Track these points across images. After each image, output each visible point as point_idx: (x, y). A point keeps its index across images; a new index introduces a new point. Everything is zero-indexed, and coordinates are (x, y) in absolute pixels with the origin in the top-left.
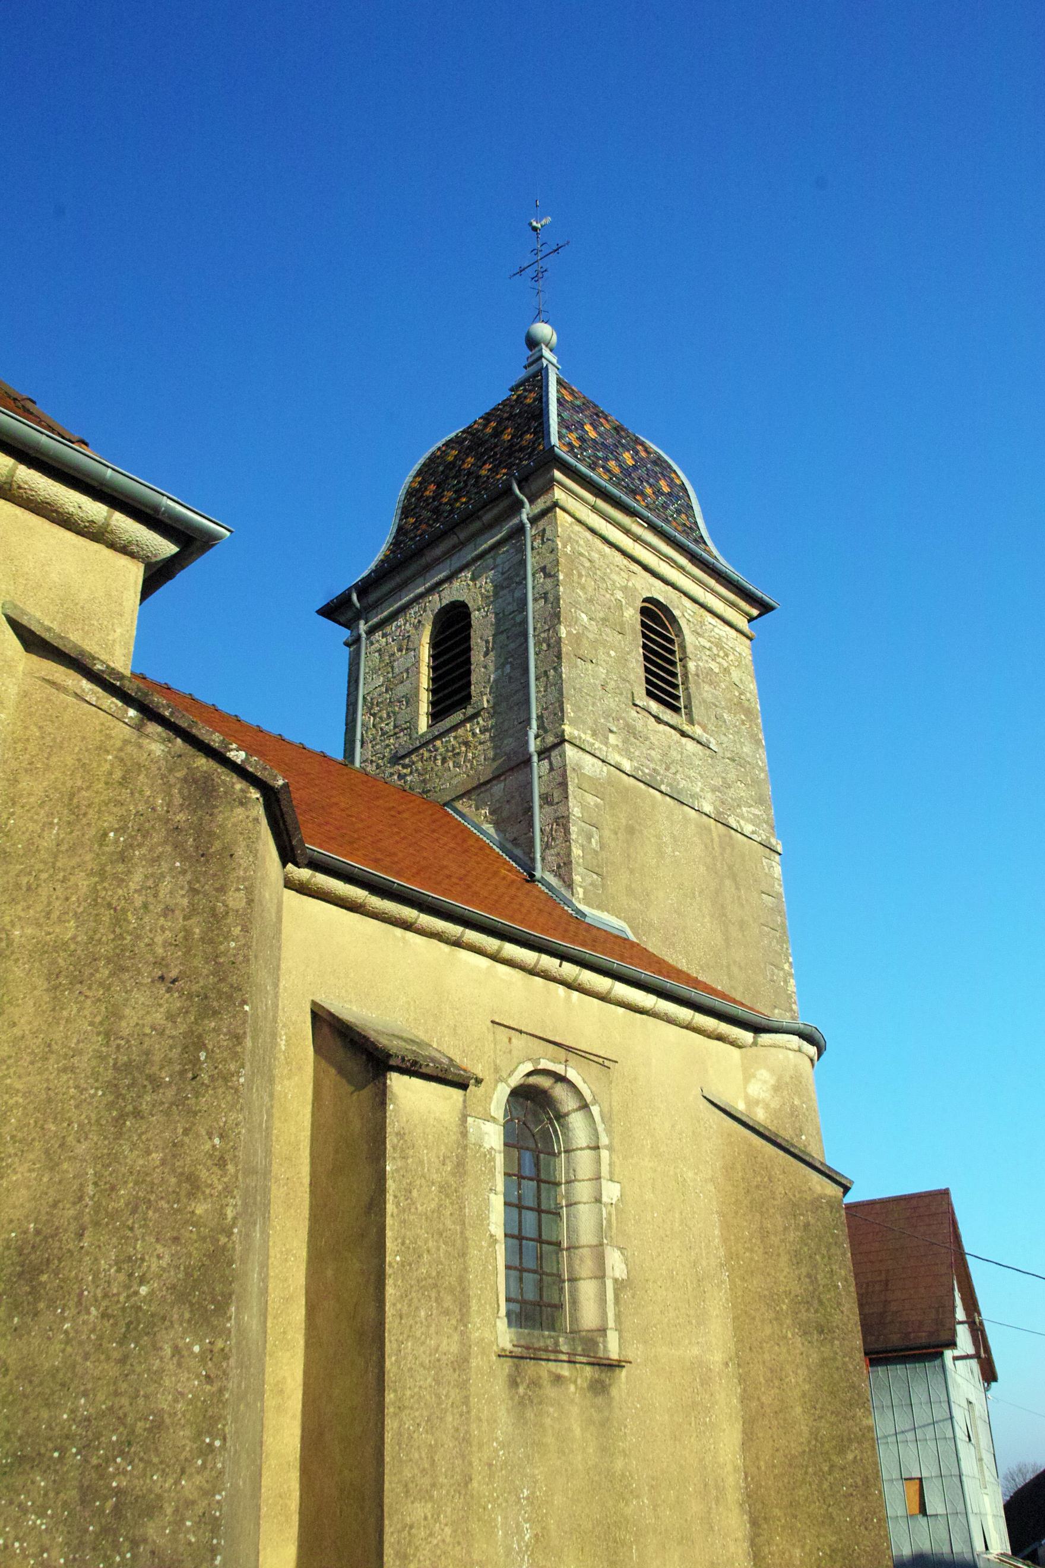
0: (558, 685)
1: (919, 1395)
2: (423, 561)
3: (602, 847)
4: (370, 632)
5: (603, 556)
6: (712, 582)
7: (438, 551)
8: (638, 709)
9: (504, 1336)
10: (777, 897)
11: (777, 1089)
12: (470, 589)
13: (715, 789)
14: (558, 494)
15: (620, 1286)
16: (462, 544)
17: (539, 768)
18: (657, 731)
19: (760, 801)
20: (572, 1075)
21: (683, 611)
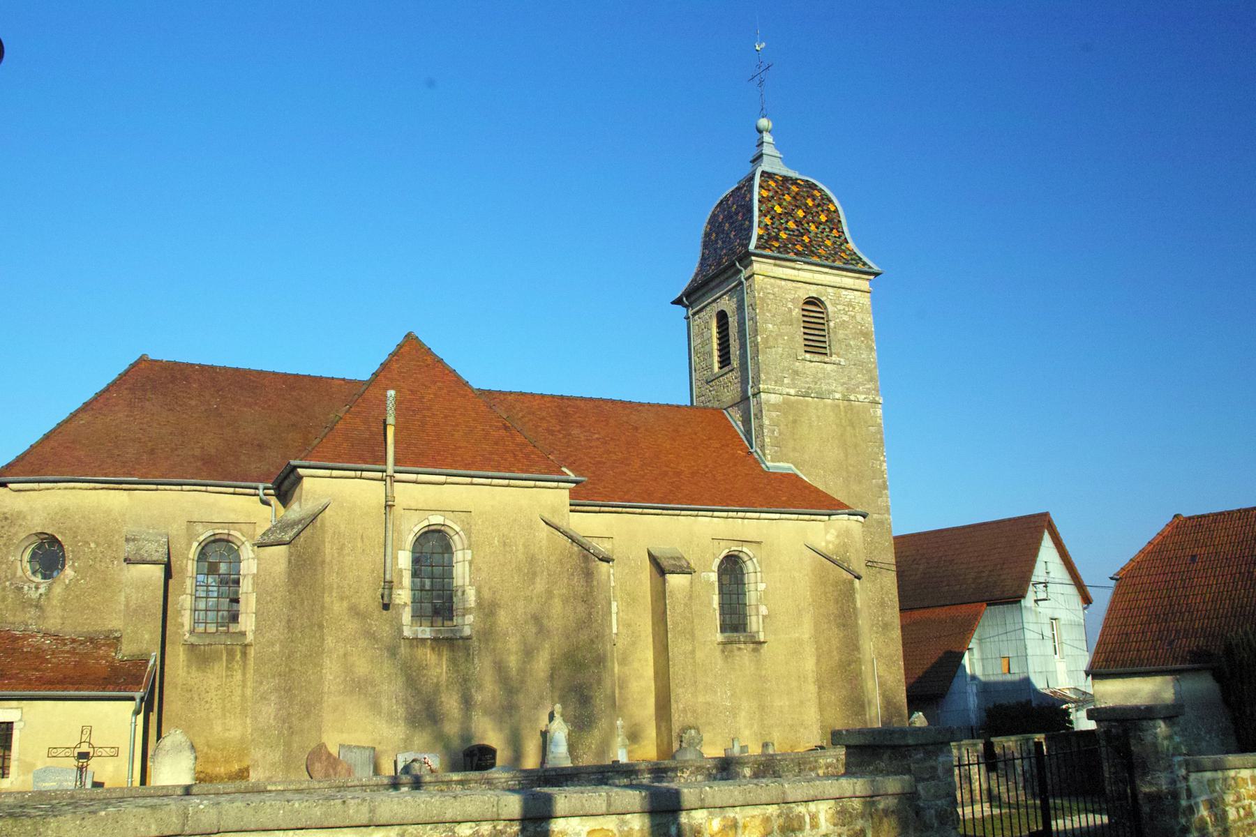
0: (757, 363)
1: (1009, 620)
3: (780, 434)
4: (694, 314)
5: (780, 287)
7: (714, 284)
9: (719, 637)
10: (879, 425)
11: (838, 536)
15: (765, 617)
16: (722, 283)
17: (753, 402)
18: (812, 366)
20: (745, 549)
21: (828, 296)
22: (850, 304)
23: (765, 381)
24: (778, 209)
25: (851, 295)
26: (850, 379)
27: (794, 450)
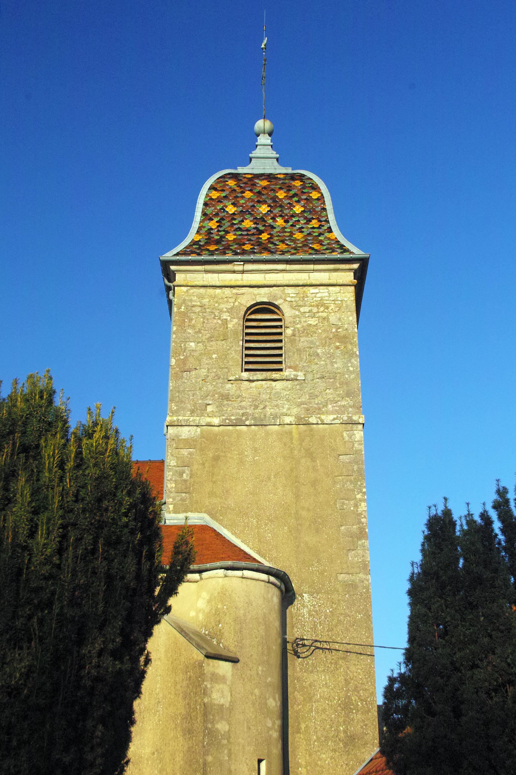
6: (311, 267)
8: (232, 382)
10: (358, 452)
11: (209, 601)
13: (299, 405)
14: (180, 278)
19: (348, 394)
22: (321, 304)
23: (174, 413)
24: (231, 209)
25: (323, 292)
26: (313, 396)
27: (212, 494)
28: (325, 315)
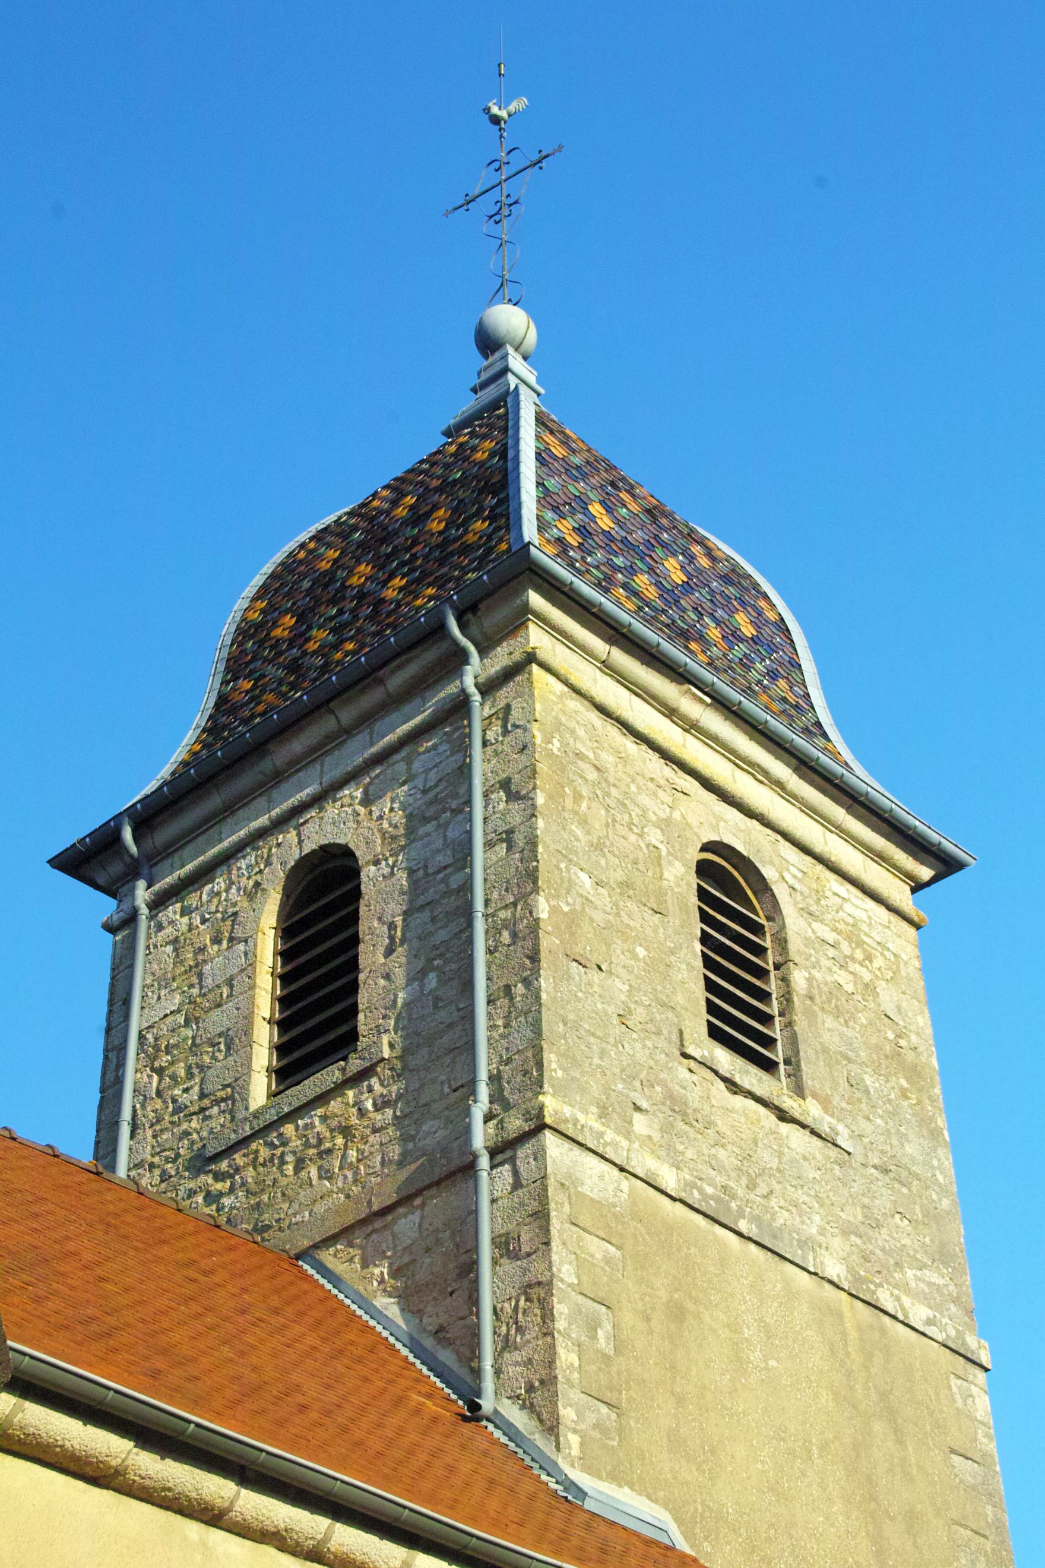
2: (266, 765)
4: (158, 903)
5: (623, 759)
6: (839, 813)
7: (297, 745)
12: (356, 821)
14: (536, 637)
17: (492, 1182)
19: (942, 1256)
23: (561, 1091)
28: (867, 977)
